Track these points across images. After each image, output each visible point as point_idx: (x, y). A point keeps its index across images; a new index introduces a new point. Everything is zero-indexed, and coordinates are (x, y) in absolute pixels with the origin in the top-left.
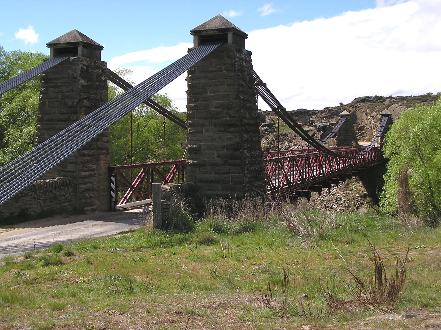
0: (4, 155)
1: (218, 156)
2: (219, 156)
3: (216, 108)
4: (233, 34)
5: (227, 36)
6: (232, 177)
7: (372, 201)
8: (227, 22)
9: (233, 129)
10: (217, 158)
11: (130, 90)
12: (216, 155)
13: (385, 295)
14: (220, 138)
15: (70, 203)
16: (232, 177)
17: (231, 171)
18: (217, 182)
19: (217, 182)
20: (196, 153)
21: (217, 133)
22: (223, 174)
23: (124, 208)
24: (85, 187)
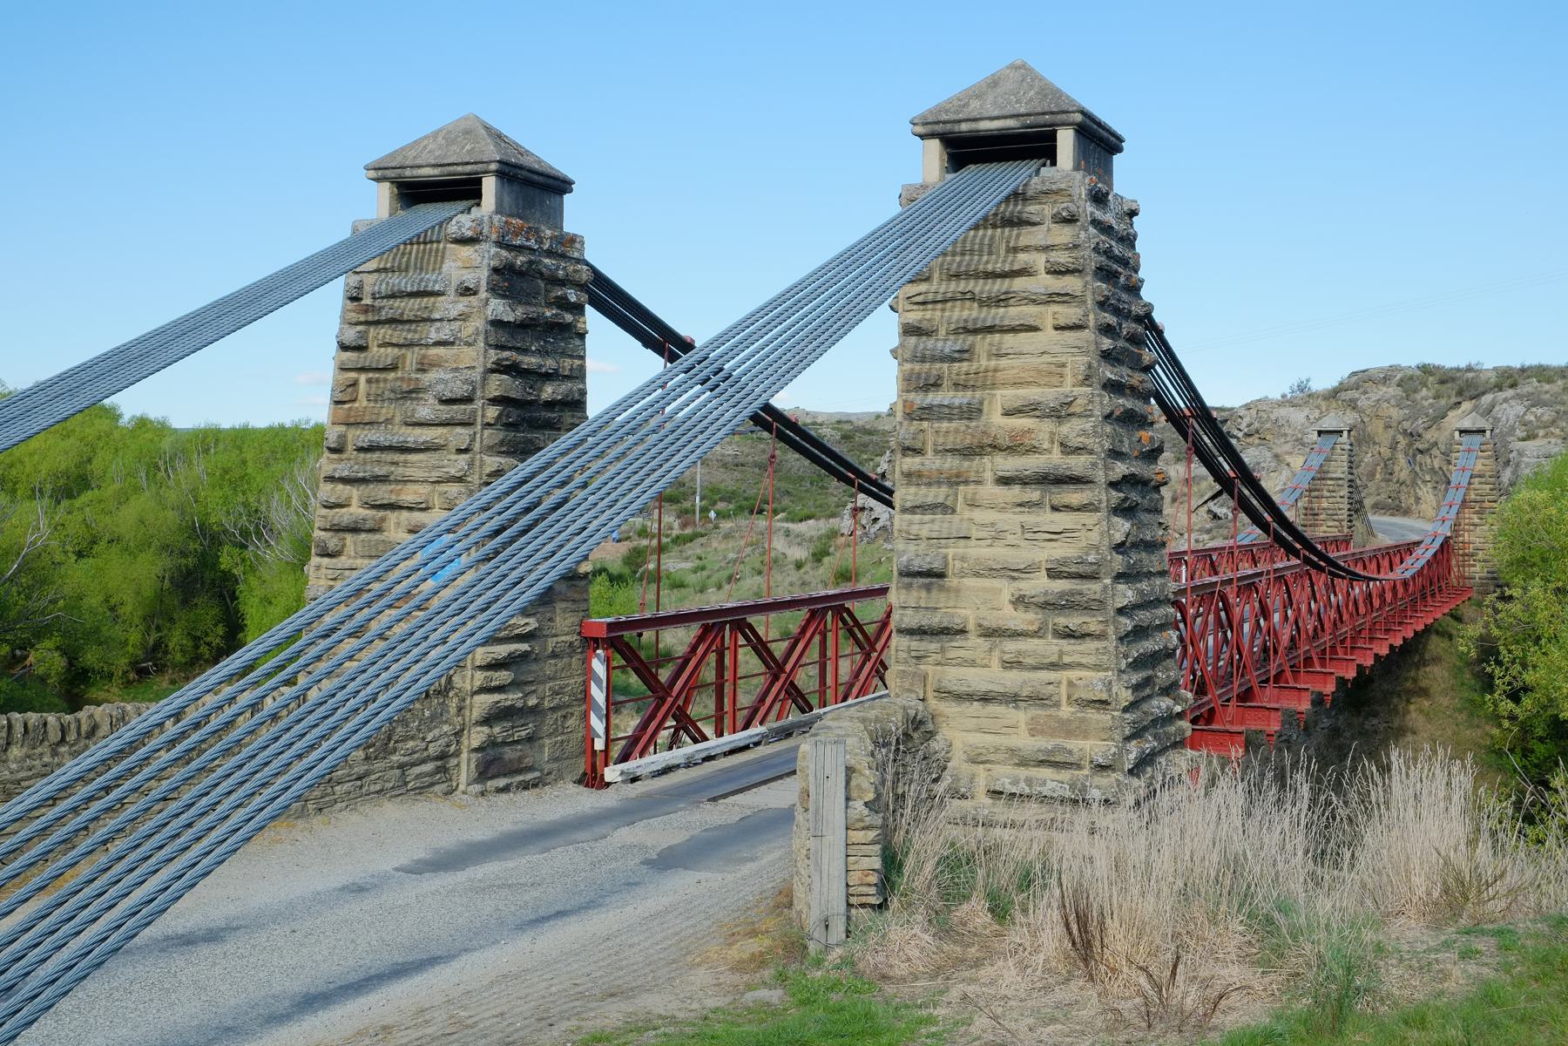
0: (1494, 710)
1: (1018, 599)
2: (1020, 601)
3: (1008, 413)
4: (1076, 131)
5: (1054, 139)
6: (1071, 684)
7: (1399, 733)
8: (1057, 94)
9: (1075, 496)
10: (1010, 606)
11: (686, 359)
12: (1006, 596)
13: (871, 437)
14: (1023, 533)
15: (439, 763)
16: (1071, 684)
17: (1067, 659)
18: (1014, 699)
19: (1014, 699)
20: (928, 588)
21: (1014, 513)
22: (1036, 668)
23: (1320, 632)
24: (498, 702)
